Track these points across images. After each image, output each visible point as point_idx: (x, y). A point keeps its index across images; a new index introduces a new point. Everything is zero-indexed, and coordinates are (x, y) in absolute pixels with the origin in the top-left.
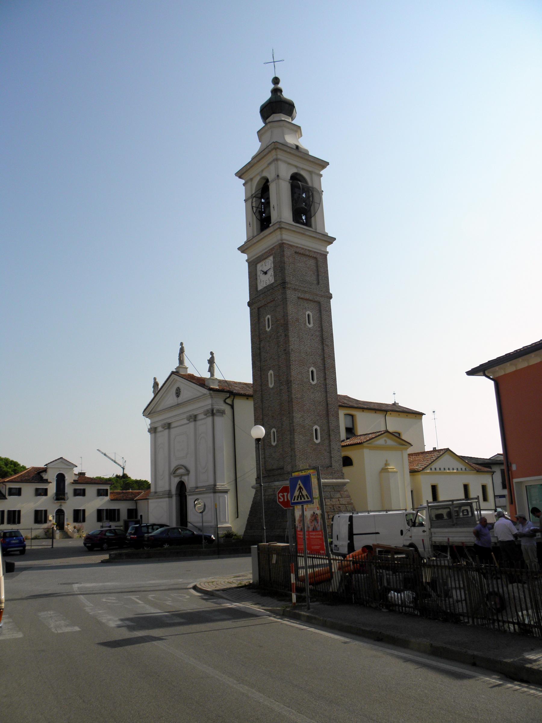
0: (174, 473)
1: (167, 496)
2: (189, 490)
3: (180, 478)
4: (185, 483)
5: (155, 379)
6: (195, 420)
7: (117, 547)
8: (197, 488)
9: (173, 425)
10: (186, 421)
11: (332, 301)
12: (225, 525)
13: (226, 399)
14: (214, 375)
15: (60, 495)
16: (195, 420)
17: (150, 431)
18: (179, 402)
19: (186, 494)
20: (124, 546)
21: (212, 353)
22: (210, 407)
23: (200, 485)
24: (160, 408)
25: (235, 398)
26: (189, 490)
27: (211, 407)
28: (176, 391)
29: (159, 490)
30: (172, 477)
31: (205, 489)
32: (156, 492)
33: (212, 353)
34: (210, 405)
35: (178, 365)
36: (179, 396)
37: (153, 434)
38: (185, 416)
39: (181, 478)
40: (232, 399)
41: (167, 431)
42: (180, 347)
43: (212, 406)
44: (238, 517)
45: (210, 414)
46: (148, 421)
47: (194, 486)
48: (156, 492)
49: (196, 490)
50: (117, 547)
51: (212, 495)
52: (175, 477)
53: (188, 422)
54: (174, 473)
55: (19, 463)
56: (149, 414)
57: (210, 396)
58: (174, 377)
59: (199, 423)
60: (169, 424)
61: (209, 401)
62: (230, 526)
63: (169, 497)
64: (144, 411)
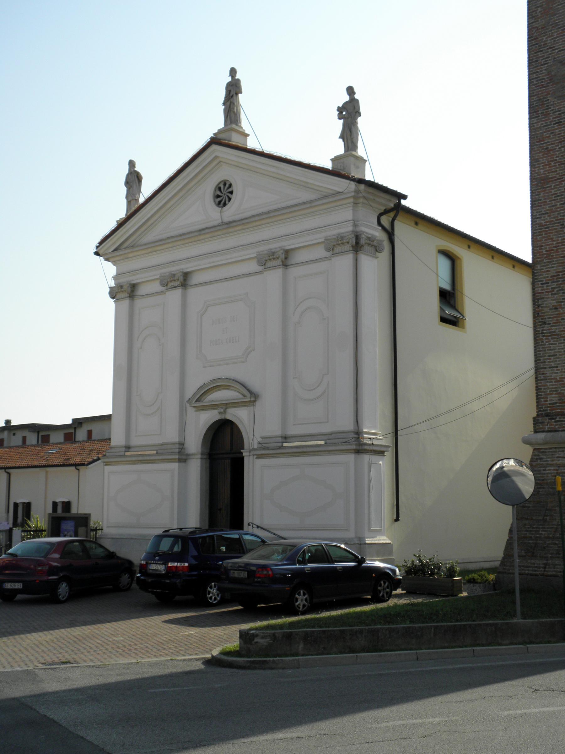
0: (198, 400)
1: (177, 457)
2: (259, 443)
3: (220, 413)
4: (240, 426)
5: (132, 164)
6: (285, 265)
7: (190, 597)
8: (286, 438)
9: (195, 279)
10: (253, 266)
11: (359, 120)
12: (378, 538)
13: (381, 215)
14: (357, 147)
15: (542, 345)
16: (285, 265)
17: (113, 293)
18: (226, 219)
19: (242, 453)
20: (150, 590)
21: (350, 91)
22: (349, 228)
23: (293, 431)
24: (150, 237)
25: (398, 218)
26: (259, 443)
27: (351, 229)
28: (215, 190)
29: (135, 441)
30: (191, 411)
31: (323, 442)
32: (128, 448)
33: (350, 91)
34: (351, 223)
35: (221, 124)
36: (225, 205)
37: (126, 303)
38: (252, 252)
39: (225, 412)
40: (391, 219)
41: (178, 292)
42: (229, 79)
43: (355, 225)
44: (397, 520)
45: (348, 247)
46: (110, 269)
47: (279, 433)
48: (128, 448)
49: (285, 444)
50: (190, 597)
51: (351, 457)
52: (199, 409)
53: (260, 268)
54: (198, 400)
55: (136, 166)
56: (116, 250)
57: (352, 200)
58: (217, 154)
59: (294, 272)
60: (186, 275)
61: (347, 214)
62: (389, 541)
63: (180, 460)
64: (101, 243)
